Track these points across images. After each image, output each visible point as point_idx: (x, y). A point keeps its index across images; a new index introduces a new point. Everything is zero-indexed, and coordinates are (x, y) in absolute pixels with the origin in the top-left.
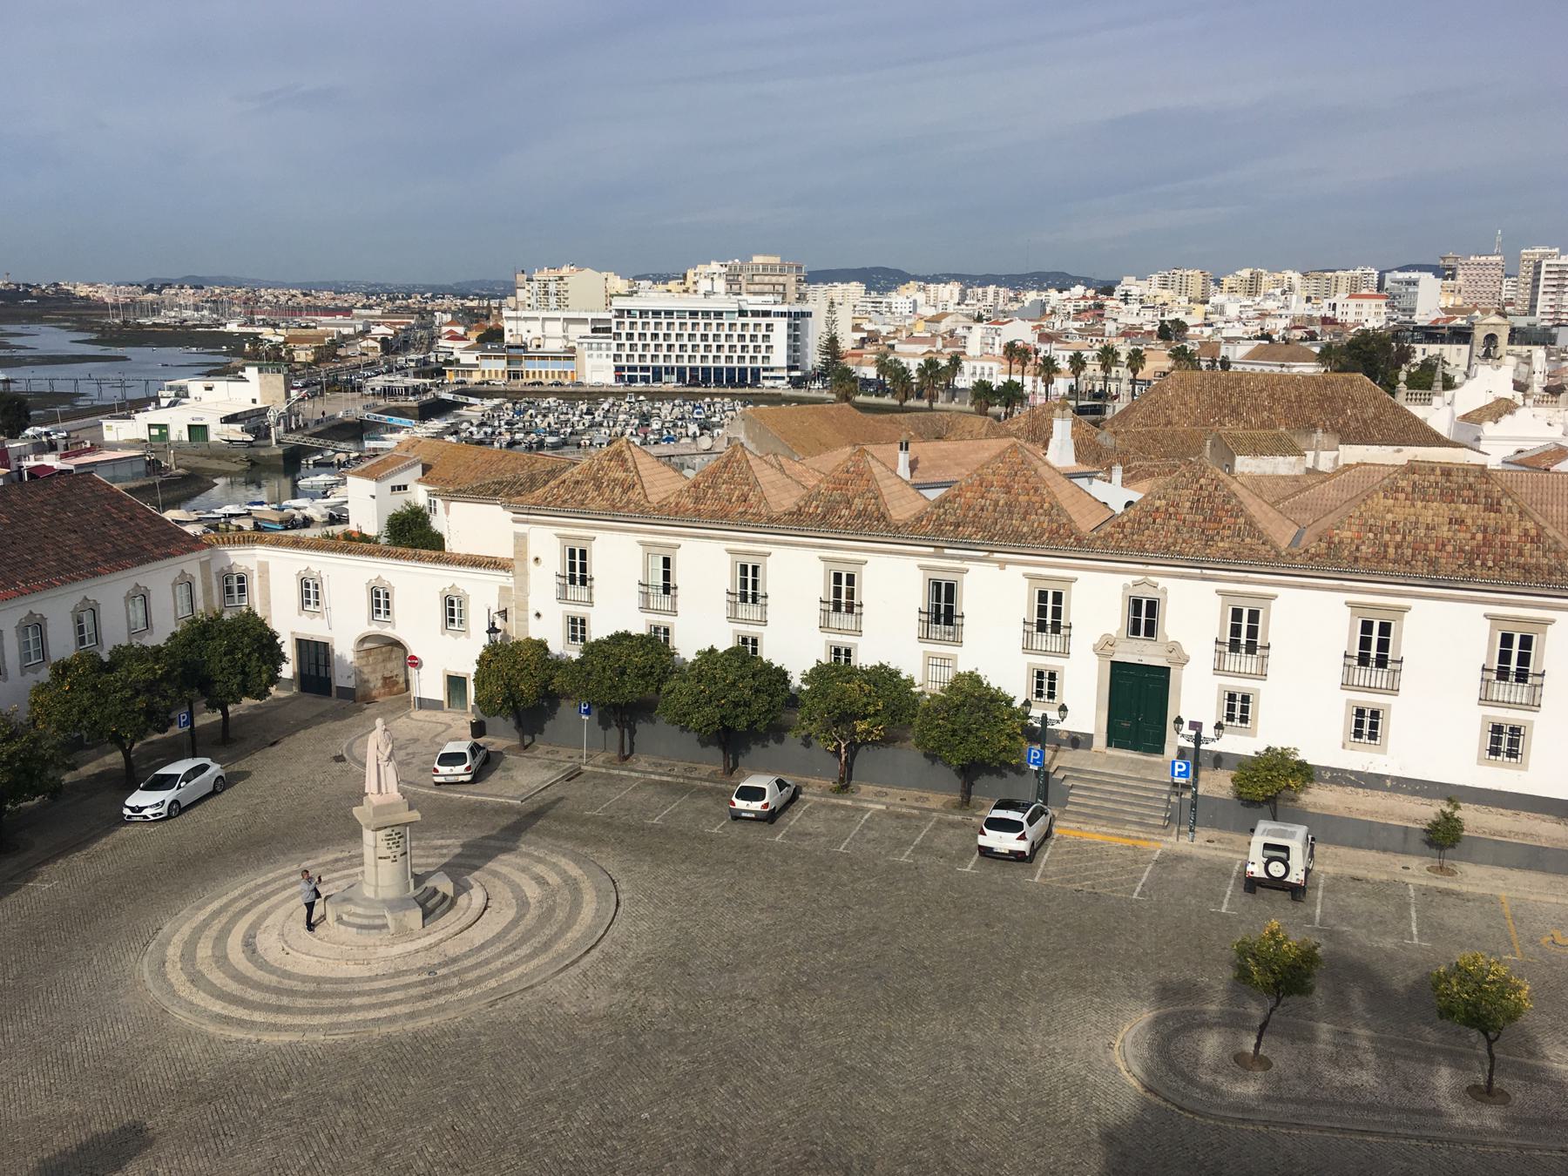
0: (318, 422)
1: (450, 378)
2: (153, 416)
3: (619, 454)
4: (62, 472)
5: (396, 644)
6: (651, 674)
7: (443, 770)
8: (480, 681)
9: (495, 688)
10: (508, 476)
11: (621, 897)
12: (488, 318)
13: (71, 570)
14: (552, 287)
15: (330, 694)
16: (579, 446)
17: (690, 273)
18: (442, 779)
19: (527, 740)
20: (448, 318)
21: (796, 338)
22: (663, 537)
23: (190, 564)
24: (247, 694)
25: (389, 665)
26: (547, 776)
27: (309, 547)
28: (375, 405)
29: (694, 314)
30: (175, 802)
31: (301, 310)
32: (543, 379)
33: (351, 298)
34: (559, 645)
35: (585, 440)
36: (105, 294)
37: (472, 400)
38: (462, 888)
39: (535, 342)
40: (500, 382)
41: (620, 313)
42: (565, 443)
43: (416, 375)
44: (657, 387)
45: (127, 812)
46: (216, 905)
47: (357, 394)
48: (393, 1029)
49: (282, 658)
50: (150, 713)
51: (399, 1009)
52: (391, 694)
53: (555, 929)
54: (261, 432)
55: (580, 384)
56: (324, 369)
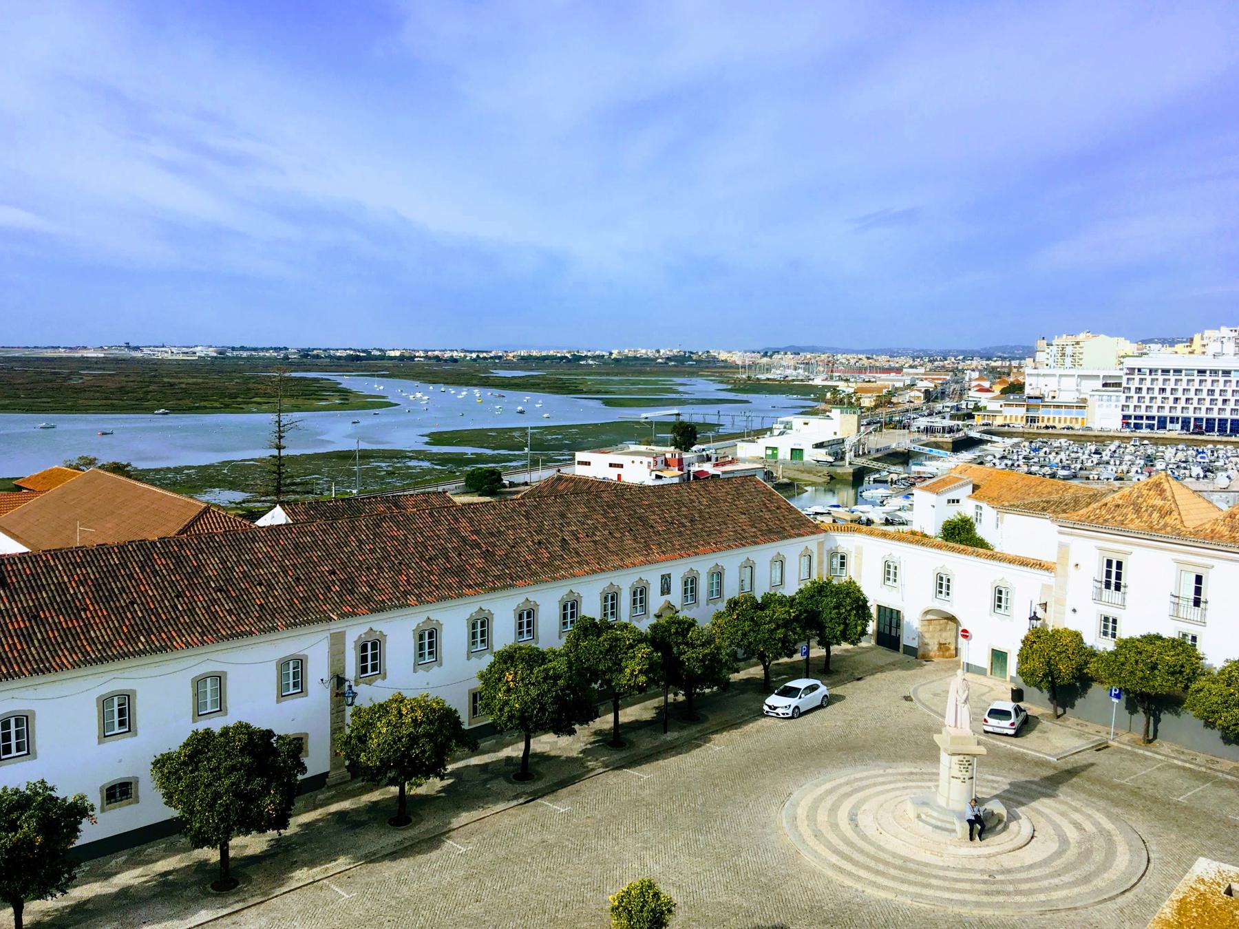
0: (878, 450)
1: (978, 420)
2: (766, 441)
3: (1158, 485)
4: (713, 476)
5: (952, 619)
6: (1181, 672)
7: (992, 721)
8: (1023, 658)
9: (1036, 664)
10: (1055, 497)
11: (1152, 856)
12: (1009, 375)
13: (742, 540)
14: (1069, 350)
15: (898, 650)
16: (1088, 478)
17: (1197, 337)
18: (990, 729)
19: (1060, 711)
20: (976, 375)
22: (1199, 559)
23: (811, 542)
24: (846, 640)
25: (944, 634)
26: (1075, 743)
27: (893, 538)
28: (919, 440)
29: (1202, 372)
30: (797, 707)
31: (866, 369)
32: (1056, 424)
33: (901, 361)
35: (1093, 474)
36: (737, 358)
37: (995, 438)
38: (1013, 817)
39: (1052, 394)
40: (1020, 425)
41: (1131, 371)
42: (1075, 476)
43: (953, 417)
44: (1161, 433)
45: (766, 708)
46: (828, 786)
47: (906, 431)
48: (964, 911)
49: (870, 617)
50: (785, 640)
51: (968, 897)
52: (943, 656)
53: (1093, 867)
54: (839, 456)
55: (1089, 429)
56: (883, 413)
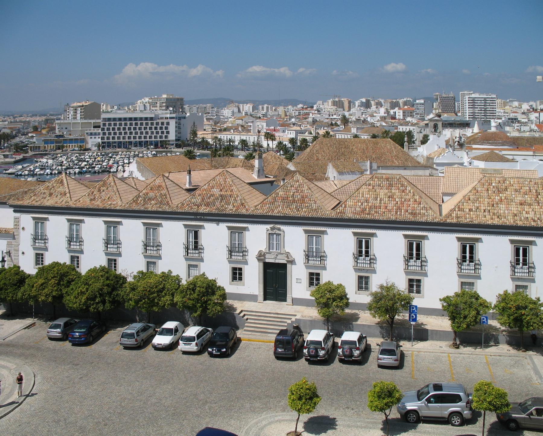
21: (179, 128)
34: (29, 267)
